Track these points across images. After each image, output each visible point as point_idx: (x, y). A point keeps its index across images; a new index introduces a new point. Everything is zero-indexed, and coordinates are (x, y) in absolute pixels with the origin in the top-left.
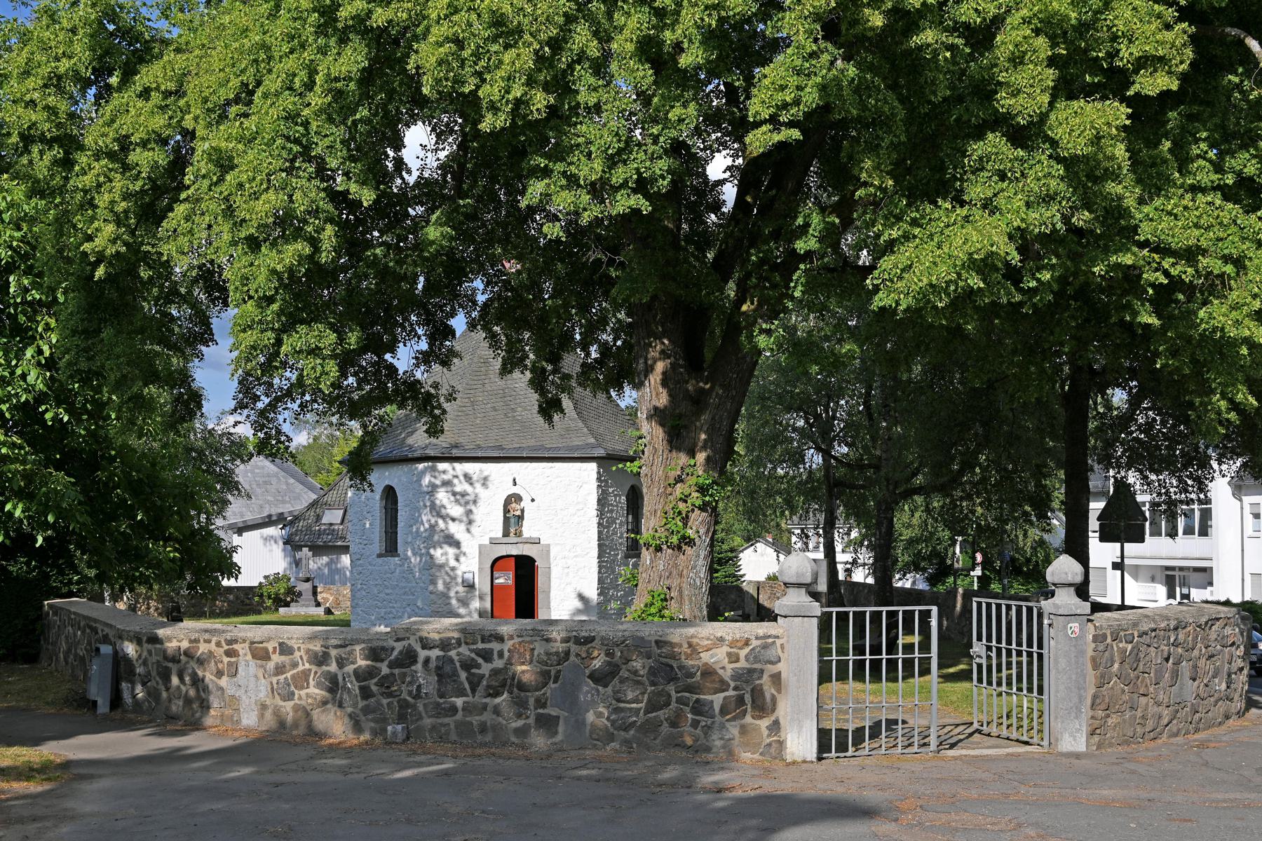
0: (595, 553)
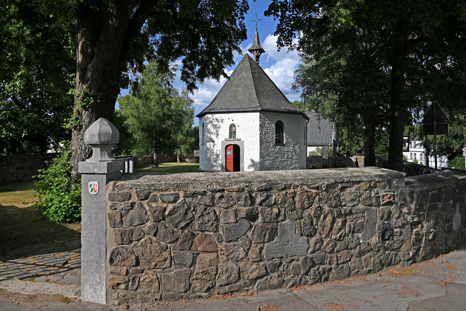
0: (259, 144)
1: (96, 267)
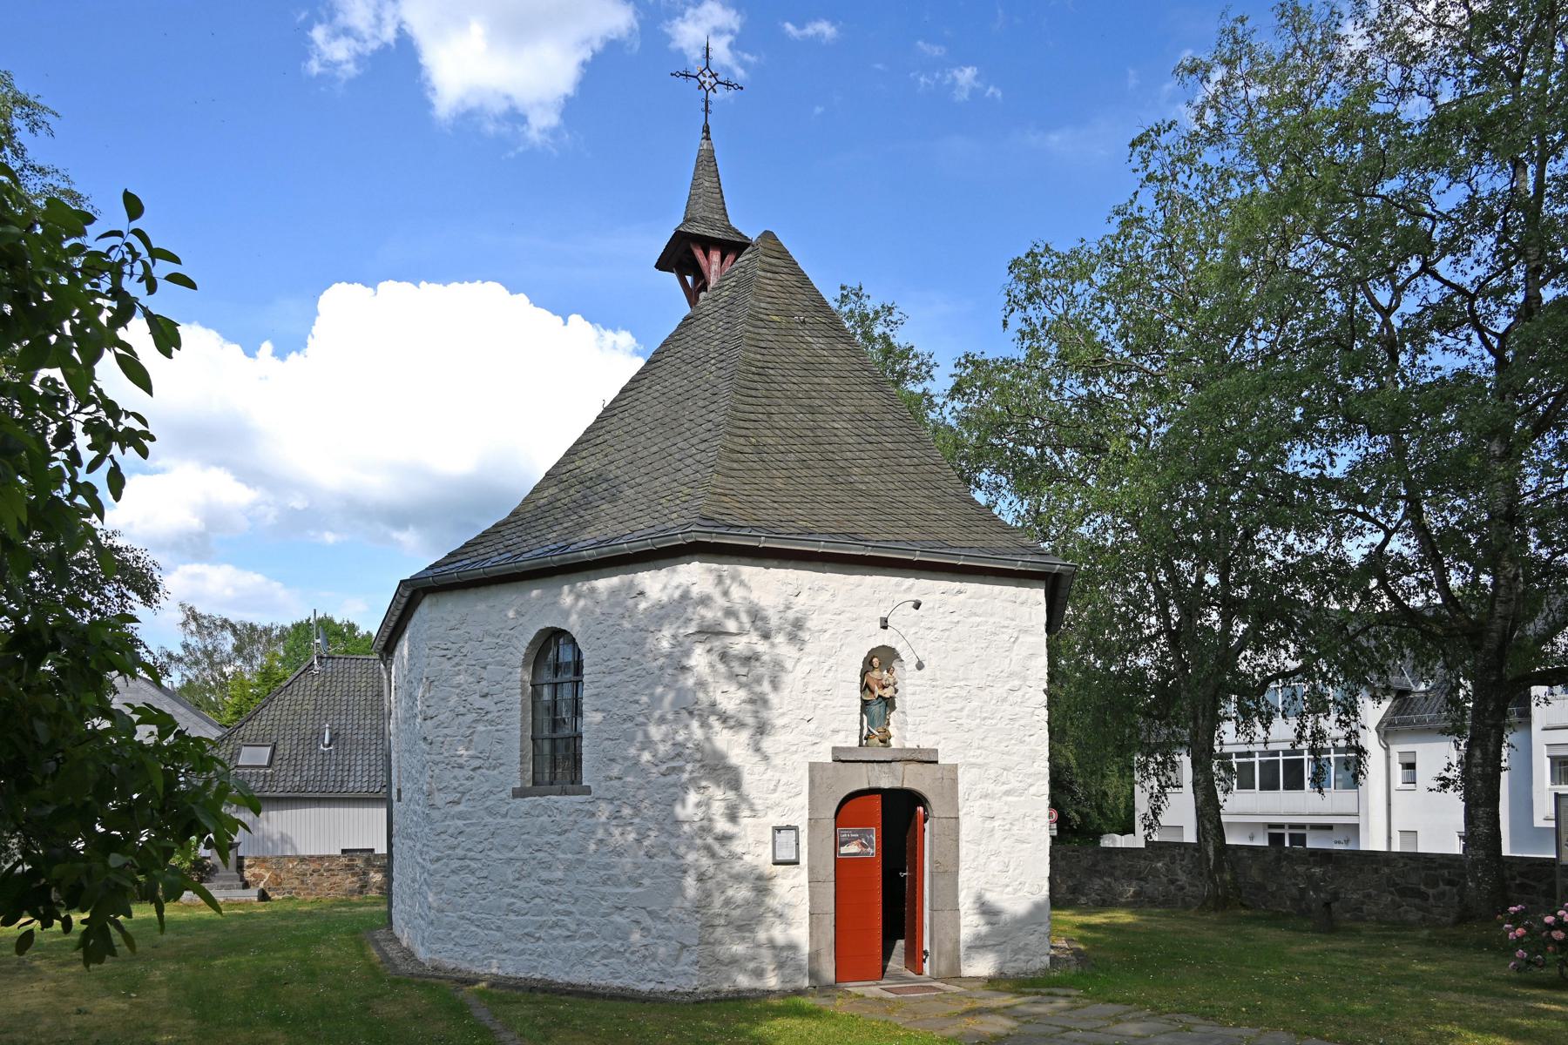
0: (1044, 787)
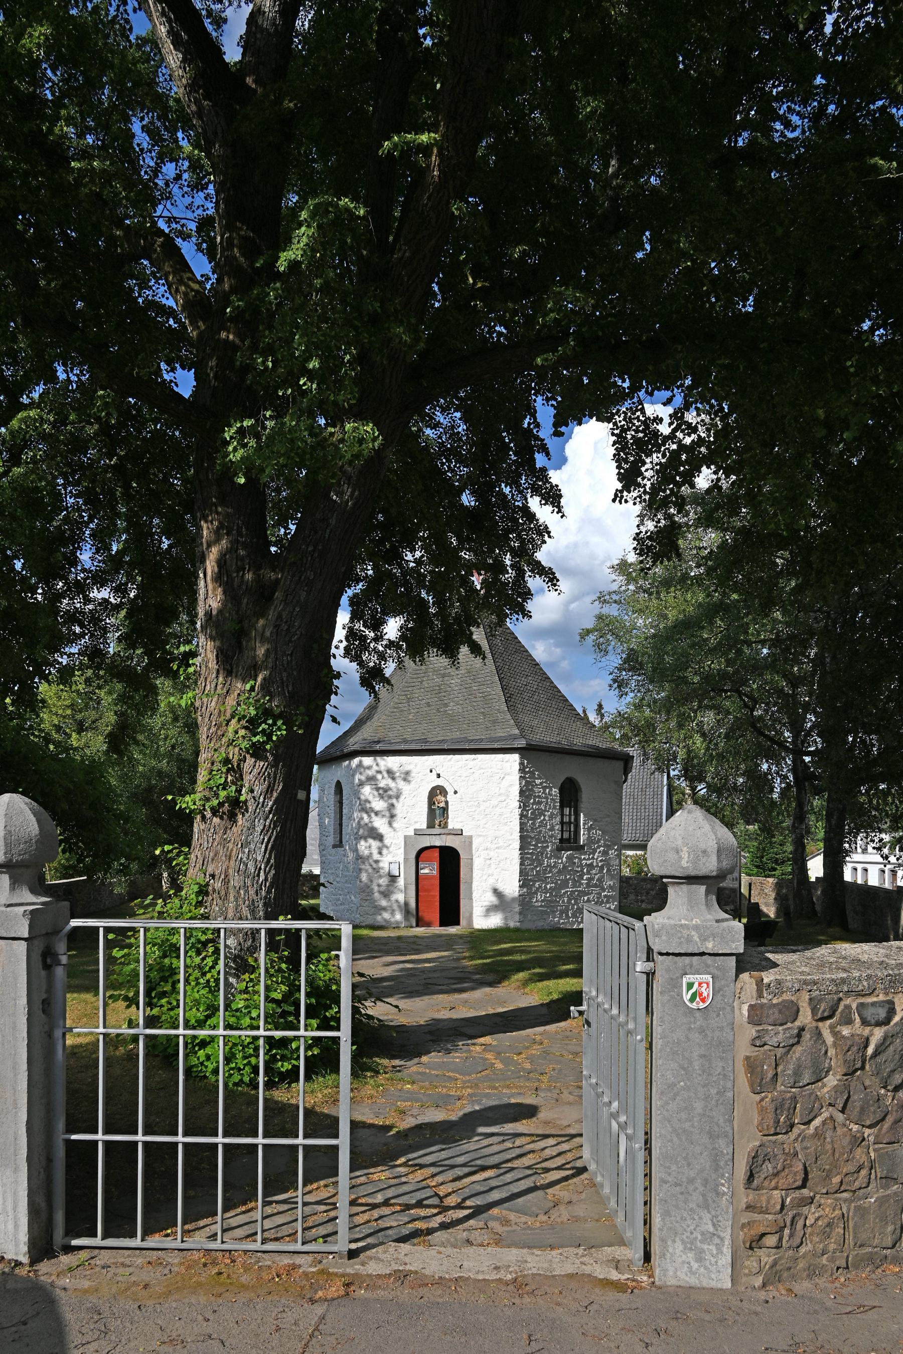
0: (517, 844)
1: (704, 1195)
